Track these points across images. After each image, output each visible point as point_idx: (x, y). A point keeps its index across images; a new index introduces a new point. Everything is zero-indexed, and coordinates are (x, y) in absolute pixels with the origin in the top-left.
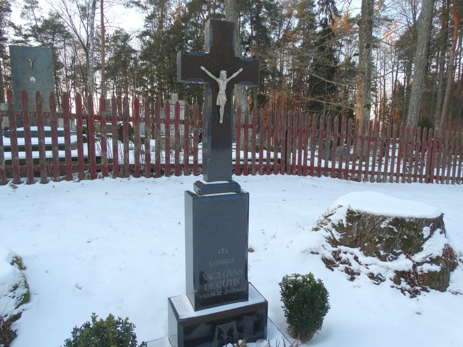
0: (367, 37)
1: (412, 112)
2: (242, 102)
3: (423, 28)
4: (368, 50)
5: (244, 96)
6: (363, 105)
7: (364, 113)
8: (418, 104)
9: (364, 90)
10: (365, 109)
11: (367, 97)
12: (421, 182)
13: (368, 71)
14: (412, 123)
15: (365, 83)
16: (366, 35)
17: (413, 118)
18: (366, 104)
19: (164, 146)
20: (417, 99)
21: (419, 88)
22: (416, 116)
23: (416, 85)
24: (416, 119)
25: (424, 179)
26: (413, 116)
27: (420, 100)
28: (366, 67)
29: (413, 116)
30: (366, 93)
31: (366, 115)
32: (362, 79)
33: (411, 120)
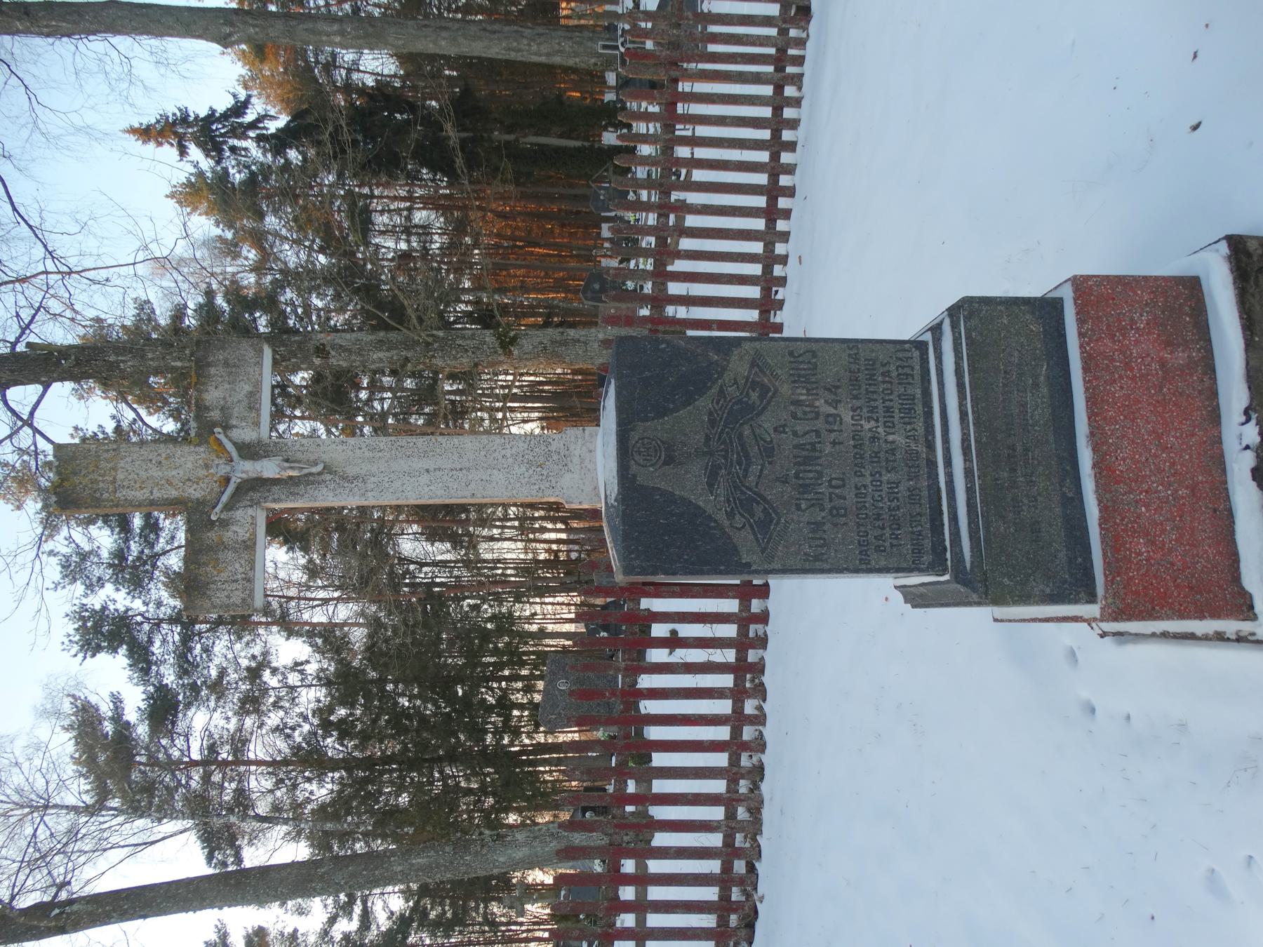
0: (295, 356)
1: (519, 50)
2: (501, 859)
3: (256, 33)
4: (333, 353)
5: (484, 851)
6: (502, 358)
7: (529, 357)
8: (496, 36)
9: (455, 358)
10: (516, 352)
11: (478, 349)
12: (801, 43)
13: (396, 348)
14: (559, 51)
15: (433, 356)
16: (289, 360)
17: (542, 48)
18: (500, 351)
19: (572, 537)
20: (480, 38)
21: (444, 34)
22: (533, 40)
23: (435, 44)
24: (542, 39)
25: (793, 33)
26: (534, 48)
27: (485, 30)
28: (387, 354)
29: (534, 48)
30: (466, 351)
31: (535, 347)
32: (424, 363)
33: (548, 55)
